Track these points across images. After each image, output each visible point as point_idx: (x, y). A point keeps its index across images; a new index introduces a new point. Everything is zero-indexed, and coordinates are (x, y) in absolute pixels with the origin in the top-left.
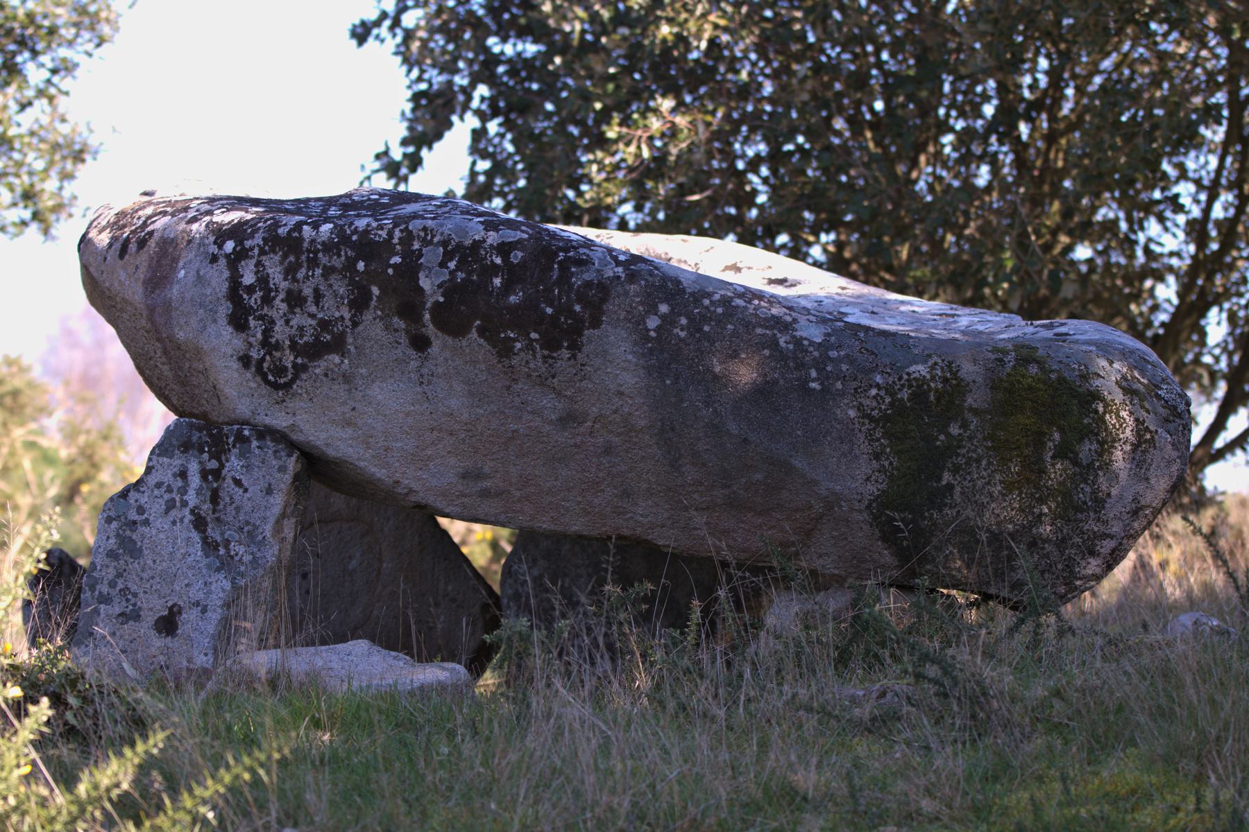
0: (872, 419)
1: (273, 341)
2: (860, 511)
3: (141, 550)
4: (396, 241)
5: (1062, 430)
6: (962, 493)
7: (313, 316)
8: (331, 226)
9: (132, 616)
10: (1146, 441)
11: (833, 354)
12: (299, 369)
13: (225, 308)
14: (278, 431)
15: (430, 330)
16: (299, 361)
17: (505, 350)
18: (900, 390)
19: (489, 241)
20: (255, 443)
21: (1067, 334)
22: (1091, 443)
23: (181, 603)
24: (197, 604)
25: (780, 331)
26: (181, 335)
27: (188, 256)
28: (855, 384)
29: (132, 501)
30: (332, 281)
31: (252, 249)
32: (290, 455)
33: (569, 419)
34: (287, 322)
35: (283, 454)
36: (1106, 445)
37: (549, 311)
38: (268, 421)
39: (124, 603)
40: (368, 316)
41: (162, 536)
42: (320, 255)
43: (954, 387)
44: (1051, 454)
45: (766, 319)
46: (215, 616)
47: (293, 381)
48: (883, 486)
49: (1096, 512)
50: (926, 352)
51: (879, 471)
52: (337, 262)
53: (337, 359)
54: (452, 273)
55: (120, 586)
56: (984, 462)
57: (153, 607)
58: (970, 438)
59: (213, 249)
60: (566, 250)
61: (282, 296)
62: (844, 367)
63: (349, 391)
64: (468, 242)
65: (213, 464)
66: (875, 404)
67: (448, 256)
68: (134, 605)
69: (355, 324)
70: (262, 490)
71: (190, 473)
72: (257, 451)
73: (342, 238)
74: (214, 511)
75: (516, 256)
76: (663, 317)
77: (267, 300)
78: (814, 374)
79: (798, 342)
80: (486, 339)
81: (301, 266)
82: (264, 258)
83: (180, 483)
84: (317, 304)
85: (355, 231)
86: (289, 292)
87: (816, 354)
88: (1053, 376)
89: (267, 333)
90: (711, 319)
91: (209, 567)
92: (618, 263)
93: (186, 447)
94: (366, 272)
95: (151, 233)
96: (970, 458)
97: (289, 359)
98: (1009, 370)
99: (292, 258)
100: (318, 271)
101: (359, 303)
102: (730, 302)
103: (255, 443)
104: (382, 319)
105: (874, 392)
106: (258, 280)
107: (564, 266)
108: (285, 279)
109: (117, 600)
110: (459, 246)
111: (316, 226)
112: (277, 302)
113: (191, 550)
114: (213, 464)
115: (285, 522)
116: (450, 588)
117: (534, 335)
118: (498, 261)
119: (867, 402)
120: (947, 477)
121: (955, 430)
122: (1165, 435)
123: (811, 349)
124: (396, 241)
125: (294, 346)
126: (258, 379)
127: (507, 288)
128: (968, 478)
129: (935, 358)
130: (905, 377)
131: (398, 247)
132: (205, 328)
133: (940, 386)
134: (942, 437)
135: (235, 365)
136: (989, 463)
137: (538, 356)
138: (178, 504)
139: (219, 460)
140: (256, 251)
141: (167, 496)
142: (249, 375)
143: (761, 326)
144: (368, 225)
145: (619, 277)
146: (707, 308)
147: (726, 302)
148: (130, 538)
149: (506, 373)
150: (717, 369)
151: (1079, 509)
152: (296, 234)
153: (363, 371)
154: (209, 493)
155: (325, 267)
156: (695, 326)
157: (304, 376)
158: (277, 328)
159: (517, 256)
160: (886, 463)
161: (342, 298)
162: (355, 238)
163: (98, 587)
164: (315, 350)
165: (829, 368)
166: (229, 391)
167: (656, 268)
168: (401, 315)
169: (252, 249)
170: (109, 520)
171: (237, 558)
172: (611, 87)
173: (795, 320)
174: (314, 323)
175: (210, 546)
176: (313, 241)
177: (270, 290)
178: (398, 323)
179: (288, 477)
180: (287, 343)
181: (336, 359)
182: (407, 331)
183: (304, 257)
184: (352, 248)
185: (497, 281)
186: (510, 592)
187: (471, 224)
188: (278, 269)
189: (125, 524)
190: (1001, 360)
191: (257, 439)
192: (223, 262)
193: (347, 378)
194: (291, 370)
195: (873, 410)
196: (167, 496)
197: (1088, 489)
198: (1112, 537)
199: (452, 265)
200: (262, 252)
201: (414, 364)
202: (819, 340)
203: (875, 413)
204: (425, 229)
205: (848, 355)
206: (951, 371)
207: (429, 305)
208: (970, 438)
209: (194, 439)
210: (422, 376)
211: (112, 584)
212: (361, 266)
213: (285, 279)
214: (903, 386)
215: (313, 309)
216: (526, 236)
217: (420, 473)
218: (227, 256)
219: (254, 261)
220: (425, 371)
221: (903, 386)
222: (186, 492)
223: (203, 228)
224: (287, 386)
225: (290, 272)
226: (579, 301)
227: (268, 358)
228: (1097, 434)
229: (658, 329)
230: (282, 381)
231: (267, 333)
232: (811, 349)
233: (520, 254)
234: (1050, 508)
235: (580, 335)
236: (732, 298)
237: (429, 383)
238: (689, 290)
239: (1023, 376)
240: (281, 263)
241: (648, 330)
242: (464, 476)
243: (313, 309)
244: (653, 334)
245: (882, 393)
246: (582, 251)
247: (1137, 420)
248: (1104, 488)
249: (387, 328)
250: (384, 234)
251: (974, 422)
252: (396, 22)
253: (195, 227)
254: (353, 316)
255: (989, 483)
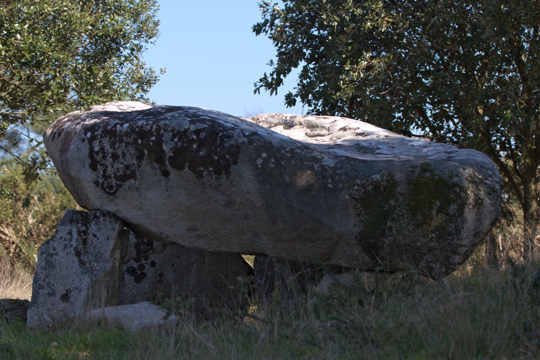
0: (356, 199)
1: (107, 174)
2: (353, 239)
3: (55, 265)
4: (154, 130)
5: (440, 200)
6: (397, 230)
7: (122, 163)
8: (128, 124)
9: (52, 294)
10: (479, 204)
11: (338, 172)
12: (118, 186)
13: (88, 161)
14: (112, 213)
15: (169, 168)
16: (118, 183)
17: (200, 176)
18: (368, 186)
19: (191, 129)
20: (102, 219)
21: (453, 157)
22: (454, 205)
23: (71, 288)
24: (77, 288)
25: (315, 163)
26: (72, 173)
27: (75, 139)
28: (348, 184)
29: (51, 245)
30: (129, 148)
31: (97, 136)
32: (116, 223)
33: (229, 204)
34: (112, 166)
35: (113, 222)
36: (462, 206)
37: (216, 158)
38: (107, 209)
39: (49, 289)
40: (144, 163)
41: (63, 260)
42: (124, 137)
43: (392, 184)
44: (436, 211)
45: (309, 158)
46: (84, 293)
47: (116, 191)
48: (362, 228)
49: (457, 235)
50: (381, 169)
51: (359, 222)
52: (131, 140)
53: (133, 181)
54: (176, 143)
55: (47, 281)
56: (406, 216)
57: (60, 290)
58: (399, 206)
59: (83, 136)
60: (223, 131)
61: (110, 155)
62: (343, 177)
63: (139, 195)
64: (182, 130)
65: (84, 228)
66: (357, 193)
67: (174, 136)
68: (53, 289)
69: (139, 166)
70: (104, 238)
71: (73, 233)
72: (102, 222)
73: (132, 129)
74: (84, 248)
75: (202, 135)
76: (264, 159)
77: (104, 157)
78: (330, 181)
79: (323, 167)
80: (192, 171)
81: (116, 142)
82: (102, 139)
83: (69, 237)
84: (124, 158)
85: (137, 127)
86: (113, 154)
87: (331, 172)
88: (436, 177)
89: (105, 171)
90: (285, 159)
91: (82, 272)
92: (245, 136)
93: (71, 221)
94: (142, 144)
95: (63, 130)
96: (399, 214)
97: (114, 182)
98: (416, 175)
99: (113, 139)
100: (123, 144)
101: (140, 157)
102: (293, 151)
103: (102, 219)
104: (149, 164)
105: (356, 187)
106: (100, 149)
107: (222, 139)
108: (111, 148)
109: (46, 287)
110: (179, 132)
111: (122, 125)
112: (108, 158)
113: (74, 265)
114: (84, 228)
115: (116, 251)
116: (233, 268)
117: (211, 169)
118: (195, 137)
119: (353, 192)
120: (389, 223)
121: (392, 202)
122: (488, 200)
123: (329, 170)
124: (154, 130)
125: (115, 176)
126: (102, 191)
127: (199, 149)
128: (399, 223)
129: (384, 172)
130: (370, 180)
131: (155, 133)
132: (80, 170)
133: (385, 184)
134: (387, 206)
135: (93, 185)
136: (408, 217)
137: (214, 177)
138: (69, 246)
139: (86, 226)
140: (99, 136)
141: (64, 243)
142: (98, 189)
143: (307, 161)
144: (143, 124)
145: (245, 142)
146: (283, 154)
147: (292, 151)
148: (51, 261)
149: (201, 185)
150: (288, 180)
151: (449, 235)
152: (114, 129)
153: (144, 186)
154: (81, 241)
155: (126, 143)
156: (278, 162)
157: (120, 189)
158: (108, 169)
159: (203, 135)
160: (363, 218)
161: (133, 155)
162: (137, 129)
163: (38, 282)
164: (124, 178)
165: (337, 178)
166: (91, 196)
167: (262, 138)
168: (157, 162)
169: (97, 136)
170: (42, 253)
171: (94, 268)
172: (350, 48)
173: (322, 158)
174: (123, 166)
175: (82, 263)
176: (121, 131)
177: (105, 153)
178: (156, 165)
179: (116, 233)
180: (113, 175)
181: (133, 181)
182: (160, 169)
183: (117, 139)
184: (136, 134)
185: (195, 146)
186: (257, 269)
187: (185, 122)
188: (108, 144)
189: (49, 255)
190: (413, 171)
191: (103, 217)
192: (86, 141)
193: (138, 189)
194: (115, 187)
195: (356, 195)
196: (64, 243)
197: (453, 226)
198: (465, 246)
199: (176, 140)
200: (102, 137)
201: (164, 183)
202: (332, 166)
203: (357, 197)
204: (165, 125)
205: (345, 172)
206: (390, 177)
207: (167, 157)
208: (399, 206)
209: (75, 218)
210: (167, 187)
211: (44, 281)
212: (140, 141)
213: (111, 148)
214: (369, 184)
215: (122, 160)
216: (207, 126)
217: (170, 229)
218: (88, 139)
219: (98, 141)
220: (168, 185)
221: (369, 184)
222: (72, 240)
223: (80, 127)
224: (114, 193)
225: (113, 145)
226: (228, 153)
227: (106, 182)
228: (456, 202)
229: (262, 164)
230: (112, 191)
231: (105, 171)
232: (329, 170)
233: (204, 134)
234: (436, 235)
235: (230, 168)
236: (294, 149)
237: (171, 190)
238: (275, 147)
239: (422, 178)
240: (109, 141)
241: (257, 165)
242: (189, 229)
243: (122, 160)
244: (260, 166)
245: (360, 188)
246: (230, 131)
247: (475, 194)
248: (460, 225)
249: (152, 168)
250: (149, 127)
251: (401, 199)
252: (272, 24)
253: (78, 126)
254: (138, 163)
255: (408, 225)
